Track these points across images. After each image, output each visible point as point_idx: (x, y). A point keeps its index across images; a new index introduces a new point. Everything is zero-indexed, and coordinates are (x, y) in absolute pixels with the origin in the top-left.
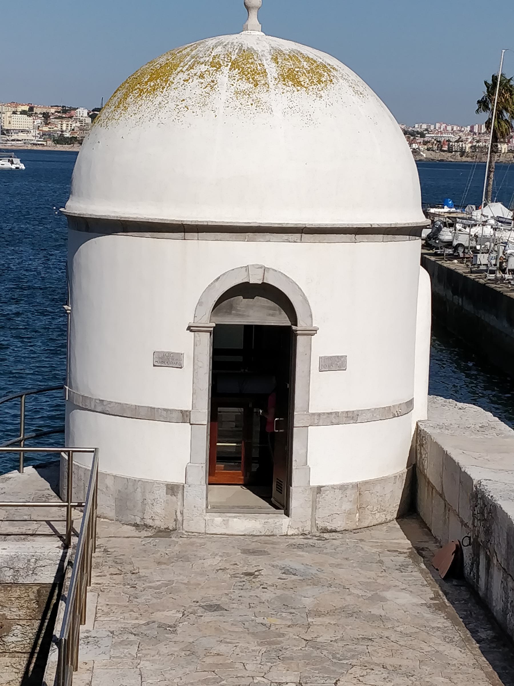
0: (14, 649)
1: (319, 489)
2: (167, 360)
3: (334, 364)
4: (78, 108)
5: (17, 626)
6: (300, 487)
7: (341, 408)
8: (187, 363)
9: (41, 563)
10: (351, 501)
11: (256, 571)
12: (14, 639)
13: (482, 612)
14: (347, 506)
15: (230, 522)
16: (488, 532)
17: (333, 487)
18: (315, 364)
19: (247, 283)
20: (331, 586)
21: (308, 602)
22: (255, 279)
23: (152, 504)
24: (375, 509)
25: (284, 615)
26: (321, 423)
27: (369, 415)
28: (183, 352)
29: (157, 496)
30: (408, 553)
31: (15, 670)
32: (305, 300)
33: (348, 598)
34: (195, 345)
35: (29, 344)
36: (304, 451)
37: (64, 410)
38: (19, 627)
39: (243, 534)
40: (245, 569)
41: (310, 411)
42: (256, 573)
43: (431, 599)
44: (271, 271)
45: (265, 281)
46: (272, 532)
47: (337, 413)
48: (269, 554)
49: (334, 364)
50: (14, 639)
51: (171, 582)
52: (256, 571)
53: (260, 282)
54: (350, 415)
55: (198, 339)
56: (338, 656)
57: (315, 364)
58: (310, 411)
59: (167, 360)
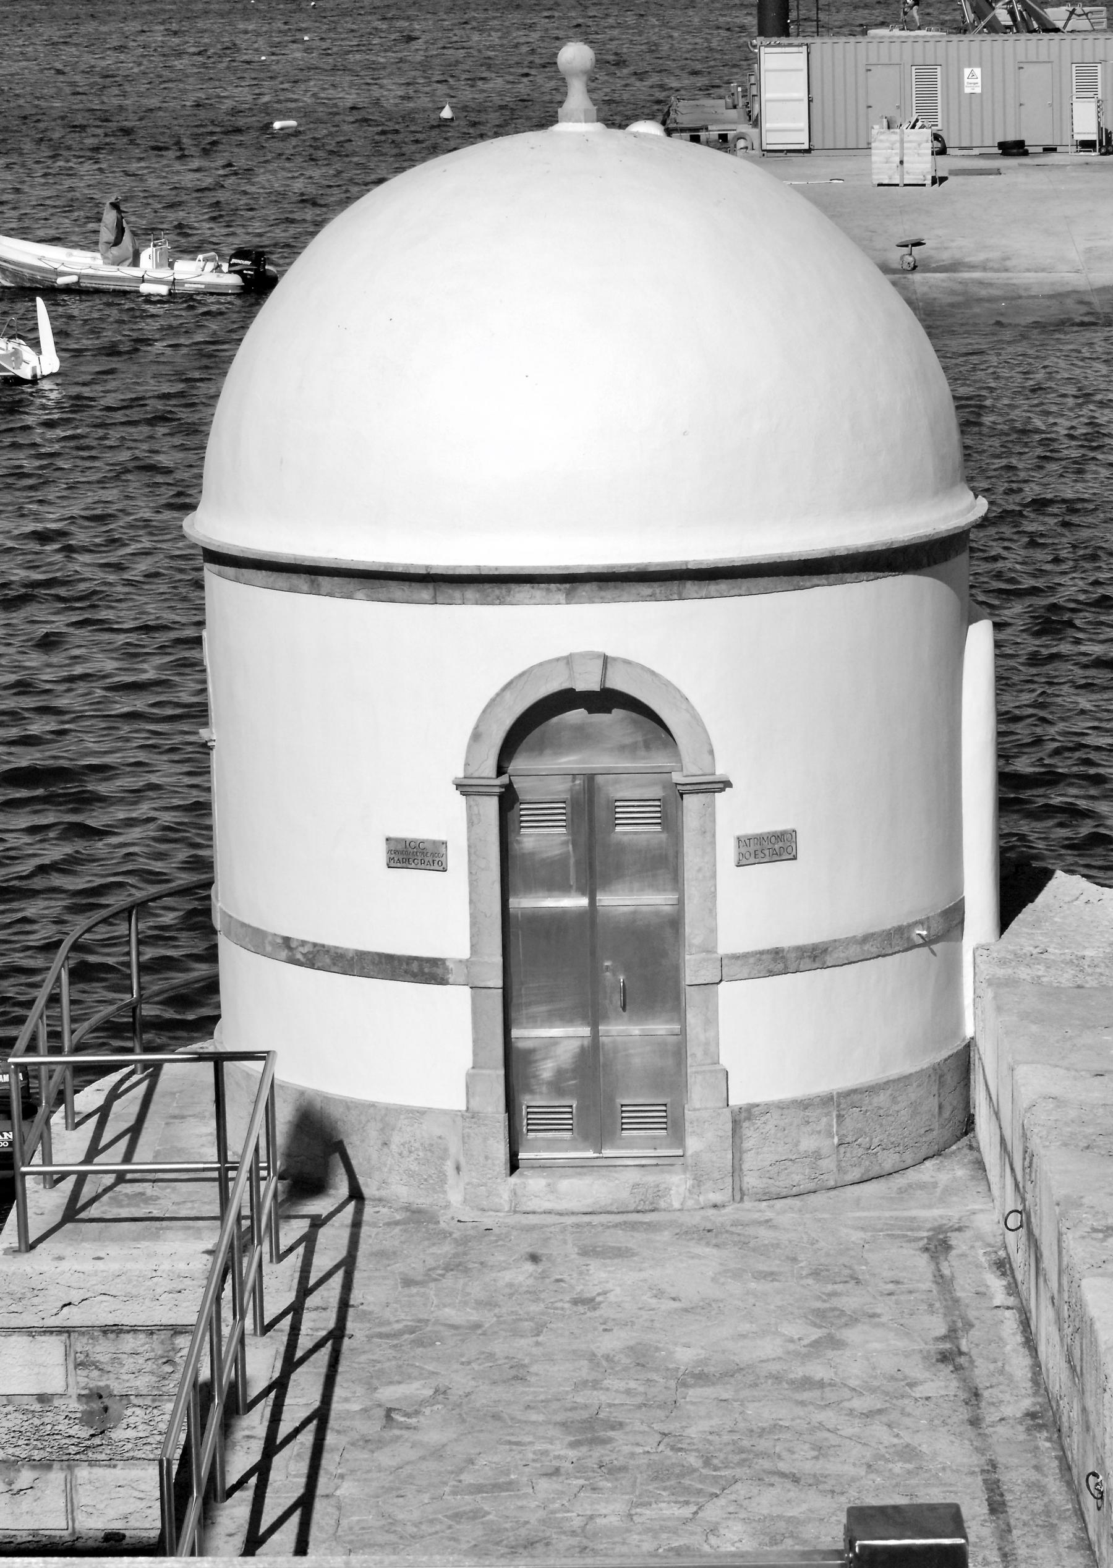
0: (131, 1454)
2: (409, 855)
5: (134, 1409)
6: (706, 1109)
8: (457, 858)
10: (819, 1132)
11: (599, 1294)
12: (131, 1433)
18: (726, 851)
19: (572, 690)
22: (587, 682)
23: (400, 1154)
24: (876, 1141)
28: (443, 839)
30: (926, 1241)
31: (136, 1494)
32: (696, 719)
35: (167, 596)
38: (138, 1411)
39: (590, 1210)
42: (599, 1299)
45: (609, 685)
46: (652, 1203)
48: (633, 1255)
50: (131, 1433)
52: (599, 1294)
53: (596, 688)
56: (715, 1461)
59: (409, 855)
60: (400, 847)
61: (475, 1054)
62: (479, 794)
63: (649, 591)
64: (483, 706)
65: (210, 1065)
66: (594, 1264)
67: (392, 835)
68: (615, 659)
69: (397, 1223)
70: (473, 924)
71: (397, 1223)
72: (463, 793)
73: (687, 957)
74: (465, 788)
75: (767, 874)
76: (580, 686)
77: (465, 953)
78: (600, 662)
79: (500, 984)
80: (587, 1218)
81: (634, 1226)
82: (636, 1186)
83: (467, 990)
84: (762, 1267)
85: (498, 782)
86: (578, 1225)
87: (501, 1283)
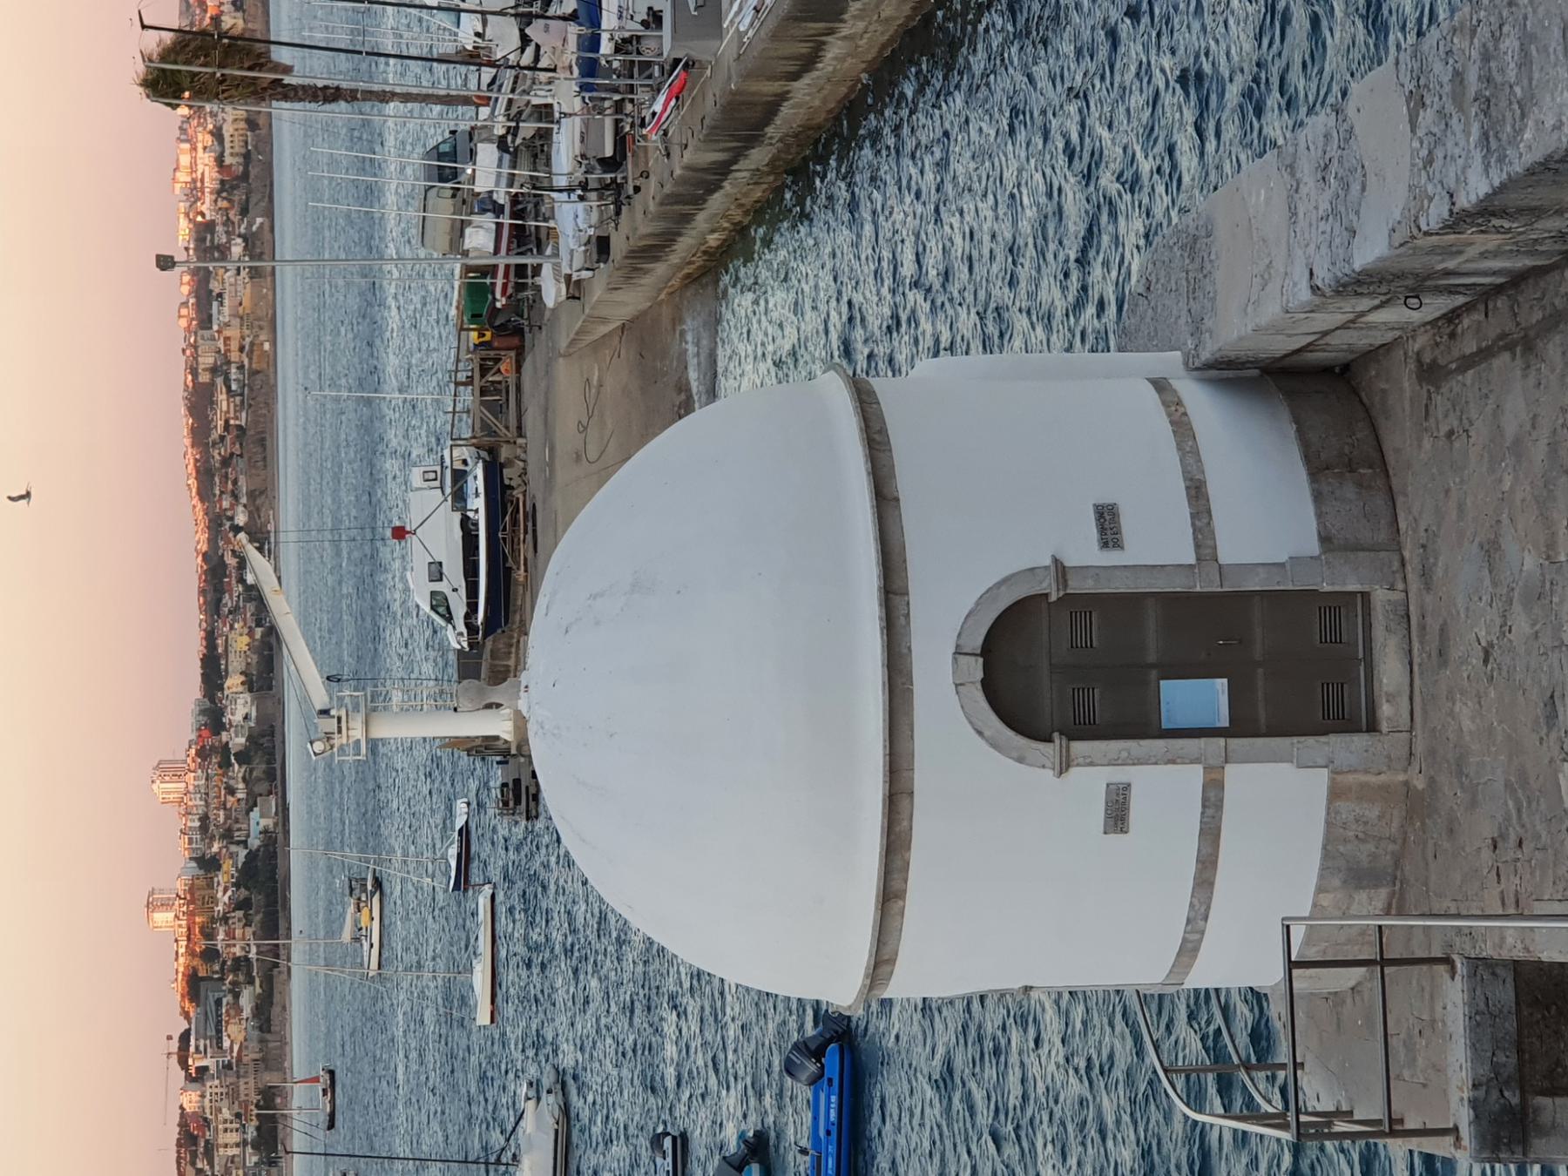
1: (1325, 539)
2: (1117, 816)
3: (1108, 524)
4: (181, 1107)
7: (1185, 511)
9: (1482, 1006)
13: (1531, 281)
14: (1349, 491)
15: (1391, 689)
16: (1400, 276)
17: (1320, 515)
18: (1112, 558)
19: (983, 682)
20: (1499, 522)
21: (1530, 562)
25: (1555, 600)
26: (1210, 542)
27: (1190, 460)
29: (1351, 818)
33: (1519, 496)
34: (1091, 764)
36: (1260, 570)
37: (1207, 990)
40: (1476, 661)
41: (1192, 560)
43: (1514, 359)
44: (961, 642)
47: (1193, 516)
49: (1108, 524)
51: (1508, 785)
53: (981, 660)
54: (1193, 492)
55: (1081, 760)
57: (1112, 558)
58: (1192, 560)
59: (1117, 816)
60: (1111, 822)
61: (1281, 761)
62: (1068, 755)
63: (902, 620)
64: (970, 604)
65: (1295, 972)
66: (1455, 653)
67: (1102, 829)
68: (957, 646)
69: (1423, 824)
70: (1173, 762)
71: (1423, 824)
72: (1068, 766)
73: (1198, 589)
74: (1064, 766)
75: (1129, 525)
76: (980, 675)
77: (1199, 769)
78: (962, 659)
79: (1222, 741)
80: (1416, 668)
81: (1423, 628)
82: (1388, 629)
83: (1228, 767)
84: (1454, 514)
85: (1057, 741)
86: (1421, 673)
87: (1473, 727)
